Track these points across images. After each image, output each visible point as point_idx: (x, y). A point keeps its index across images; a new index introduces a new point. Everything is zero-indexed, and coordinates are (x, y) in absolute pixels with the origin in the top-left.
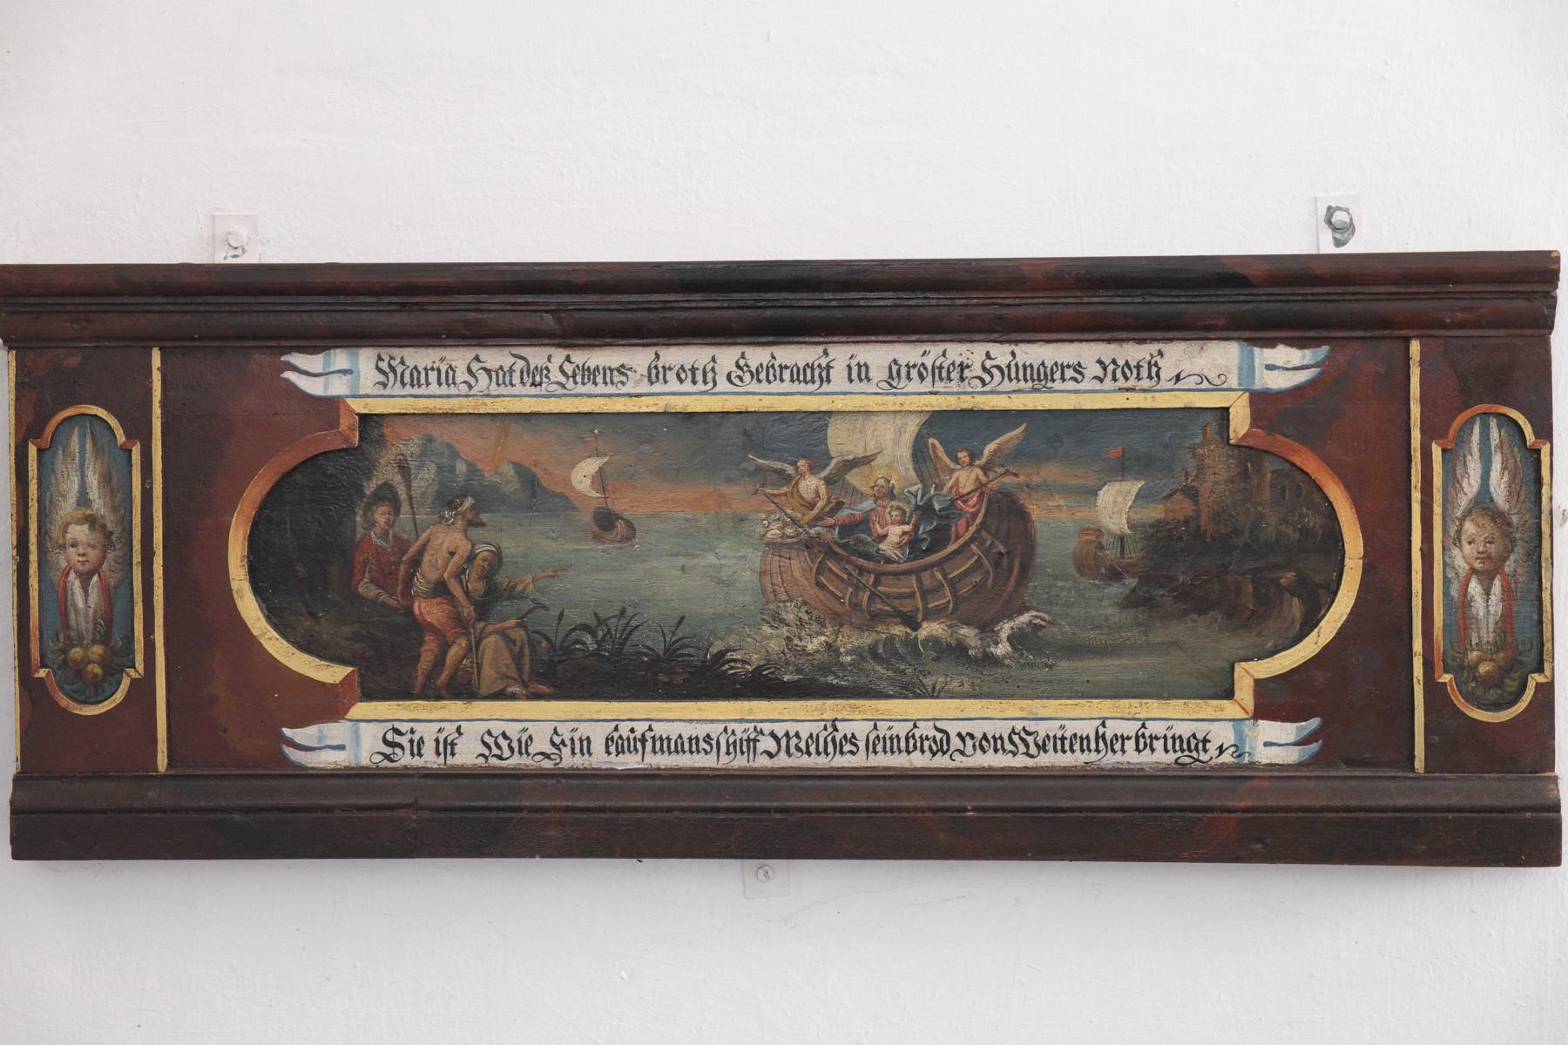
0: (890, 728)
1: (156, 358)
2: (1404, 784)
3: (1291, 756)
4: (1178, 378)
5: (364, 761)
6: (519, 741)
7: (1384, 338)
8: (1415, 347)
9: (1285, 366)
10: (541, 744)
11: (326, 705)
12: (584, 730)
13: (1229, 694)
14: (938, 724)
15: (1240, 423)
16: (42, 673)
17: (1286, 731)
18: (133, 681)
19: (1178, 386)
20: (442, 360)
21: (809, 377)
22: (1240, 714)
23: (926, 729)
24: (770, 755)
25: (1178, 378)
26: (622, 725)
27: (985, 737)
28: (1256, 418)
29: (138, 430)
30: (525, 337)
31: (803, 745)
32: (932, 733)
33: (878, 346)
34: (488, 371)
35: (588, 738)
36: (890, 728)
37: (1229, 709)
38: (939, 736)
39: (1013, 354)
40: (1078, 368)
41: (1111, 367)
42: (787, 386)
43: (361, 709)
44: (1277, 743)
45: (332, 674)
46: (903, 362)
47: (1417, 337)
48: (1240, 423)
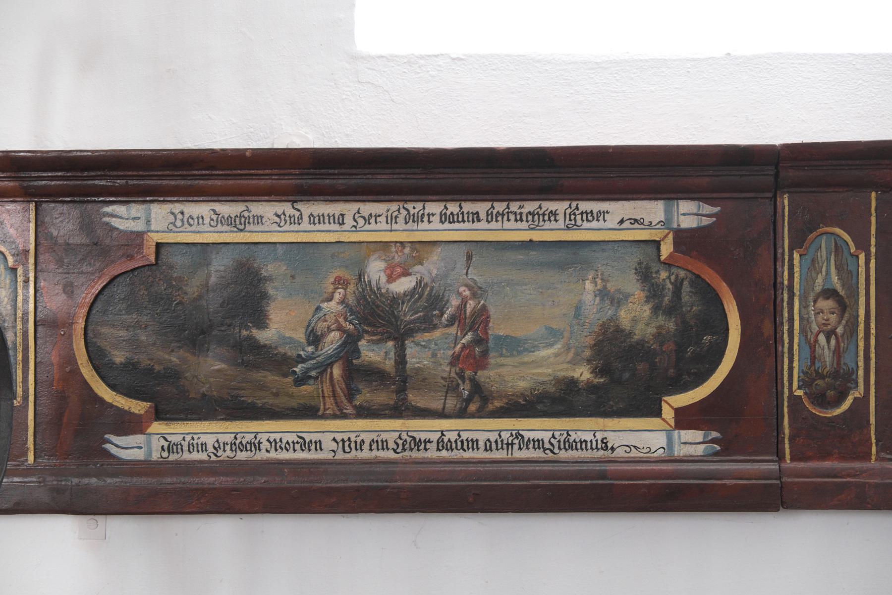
0: (199, 438)
1: (873, 194)
2: (779, 454)
3: (700, 450)
4: (622, 222)
5: (155, 456)
6: (356, 442)
7: (88, 202)
8: (873, 194)
9: (690, 214)
10: (328, 444)
11: (129, 425)
12: (204, 439)
13: (658, 413)
14: (299, 434)
15: (667, 249)
16: (799, 393)
17: (695, 435)
18: (855, 399)
19: (624, 225)
20: (520, 207)
21: (460, 219)
22: (668, 428)
23: (453, 436)
24: (267, 451)
25: (622, 222)
26: (188, 438)
27: (288, 443)
28: (676, 244)
29: (863, 245)
30: (363, 194)
31: (283, 446)
32: (296, 439)
33: (193, 204)
34: (364, 218)
35: (386, 441)
36: (199, 438)
37: (654, 422)
38: (300, 440)
39: (461, 208)
40: (554, 214)
41: (282, 217)
42: (512, 224)
43: (157, 427)
44: (692, 443)
45: (138, 407)
46: (315, 214)
47: (788, 192)
48: (667, 249)
